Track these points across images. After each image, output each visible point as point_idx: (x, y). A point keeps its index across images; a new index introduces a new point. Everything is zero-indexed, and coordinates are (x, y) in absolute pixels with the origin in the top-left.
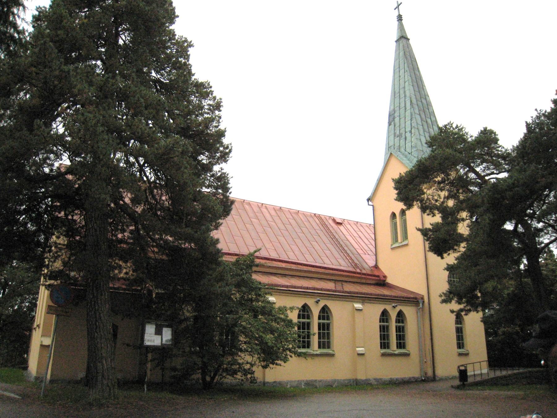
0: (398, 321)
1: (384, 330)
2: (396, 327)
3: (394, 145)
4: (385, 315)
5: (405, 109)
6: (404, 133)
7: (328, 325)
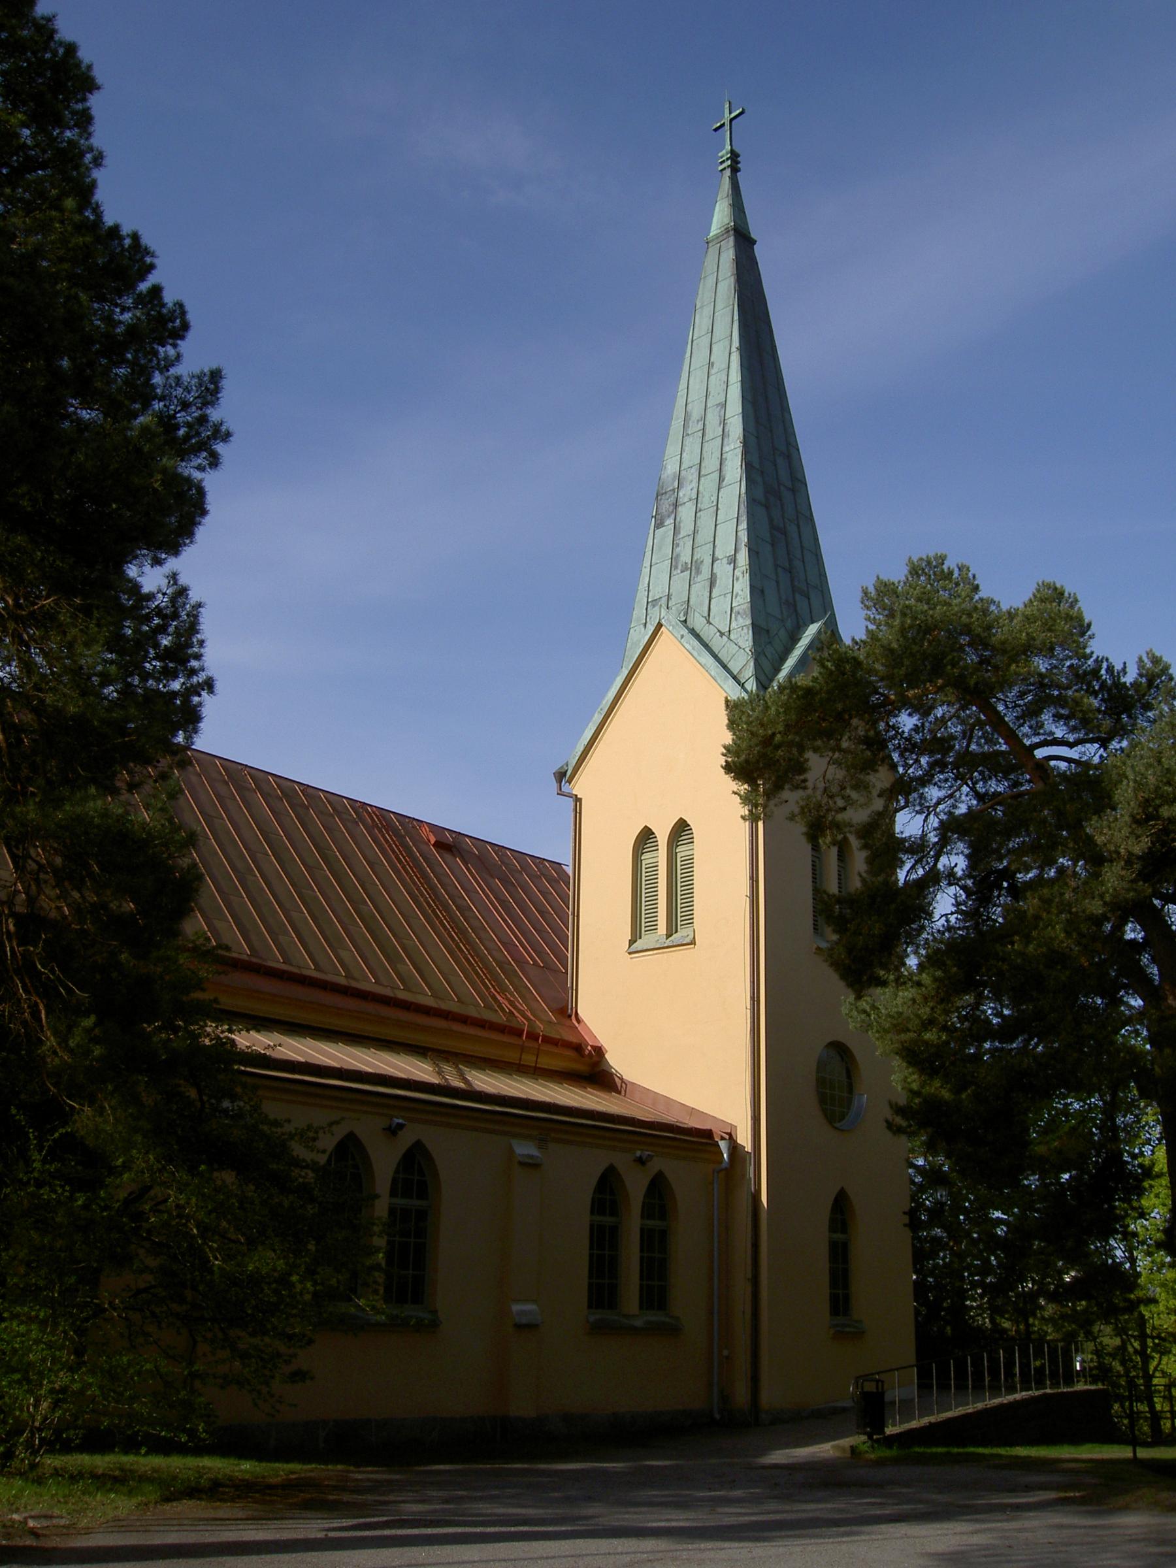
0: (648, 1211)
1: (604, 1241)
2: (642, 1230)
3: (669, 597)
4: (607, 1190)
5: (721, 479)
6: (708, 560)
7: (422, 1215)
